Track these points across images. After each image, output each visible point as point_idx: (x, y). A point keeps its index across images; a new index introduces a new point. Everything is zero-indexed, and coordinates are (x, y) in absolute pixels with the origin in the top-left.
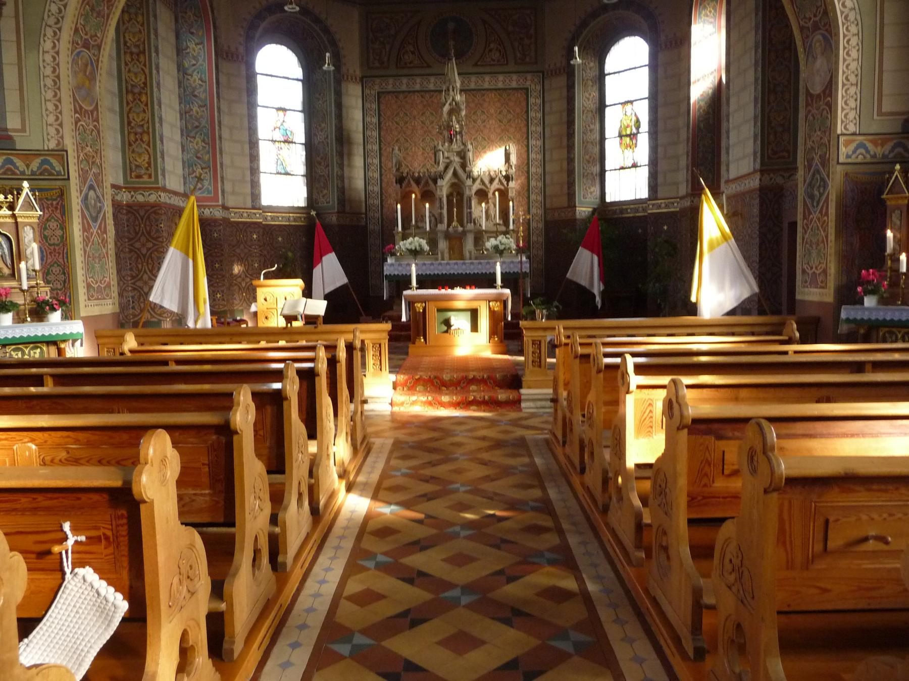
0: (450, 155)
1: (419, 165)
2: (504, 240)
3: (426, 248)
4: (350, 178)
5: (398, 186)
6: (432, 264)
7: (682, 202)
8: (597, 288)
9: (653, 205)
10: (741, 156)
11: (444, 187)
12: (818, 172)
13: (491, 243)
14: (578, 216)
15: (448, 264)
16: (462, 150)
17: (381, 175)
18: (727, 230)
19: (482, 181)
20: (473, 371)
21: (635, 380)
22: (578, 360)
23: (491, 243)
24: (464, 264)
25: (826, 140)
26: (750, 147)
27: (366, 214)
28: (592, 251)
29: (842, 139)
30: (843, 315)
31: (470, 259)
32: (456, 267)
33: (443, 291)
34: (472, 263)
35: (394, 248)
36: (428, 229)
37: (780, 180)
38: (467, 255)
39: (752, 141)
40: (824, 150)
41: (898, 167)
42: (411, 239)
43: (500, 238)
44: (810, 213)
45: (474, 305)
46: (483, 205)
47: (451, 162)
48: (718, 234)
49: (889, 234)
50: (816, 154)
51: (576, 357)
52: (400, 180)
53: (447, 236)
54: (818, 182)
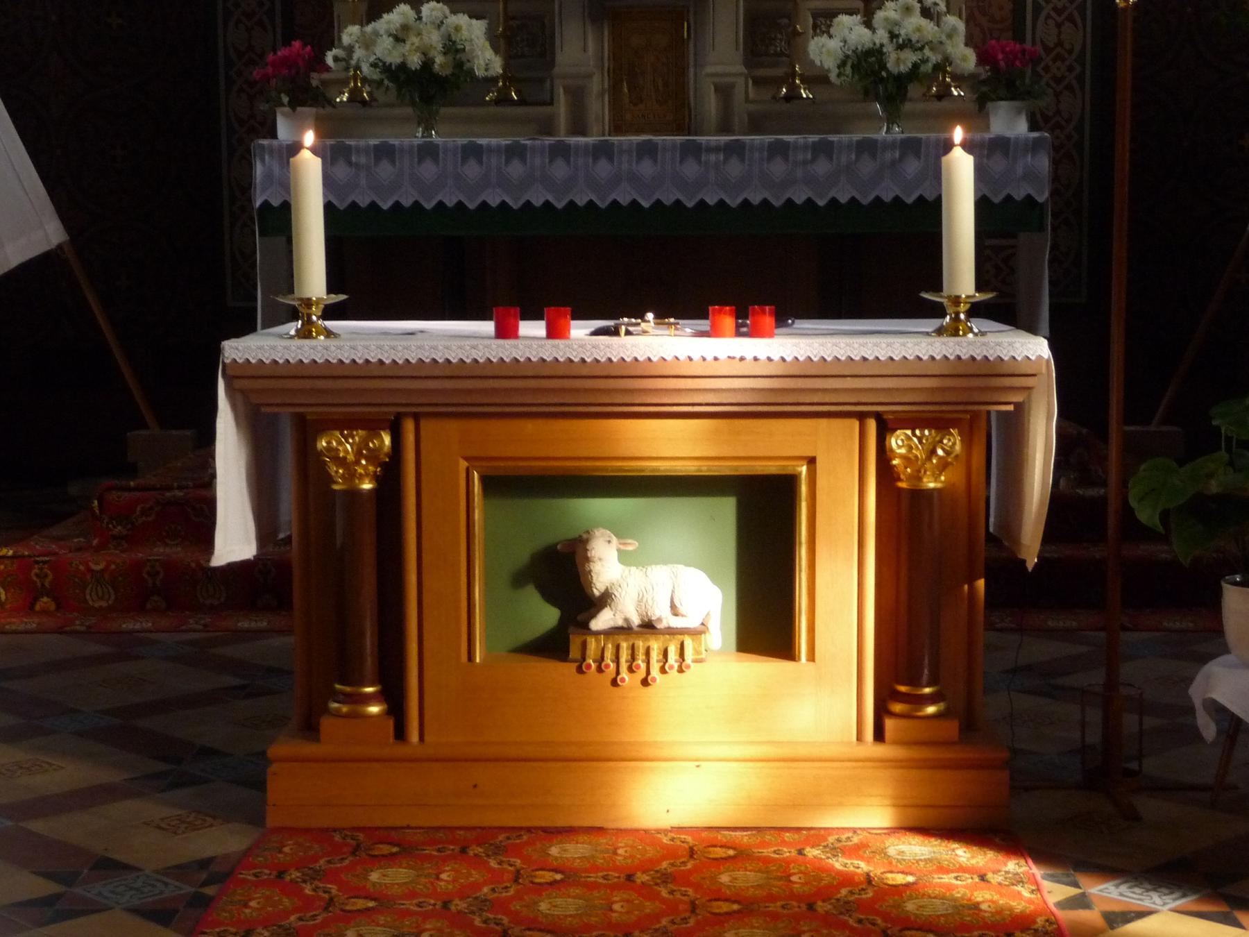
6: (515, 152)
15: (603, 151)
24: (693, 151)
31: (725, 128)
32: (646, 168)
34: (734, 150)
38: (711, 105)
45: (769, 447)
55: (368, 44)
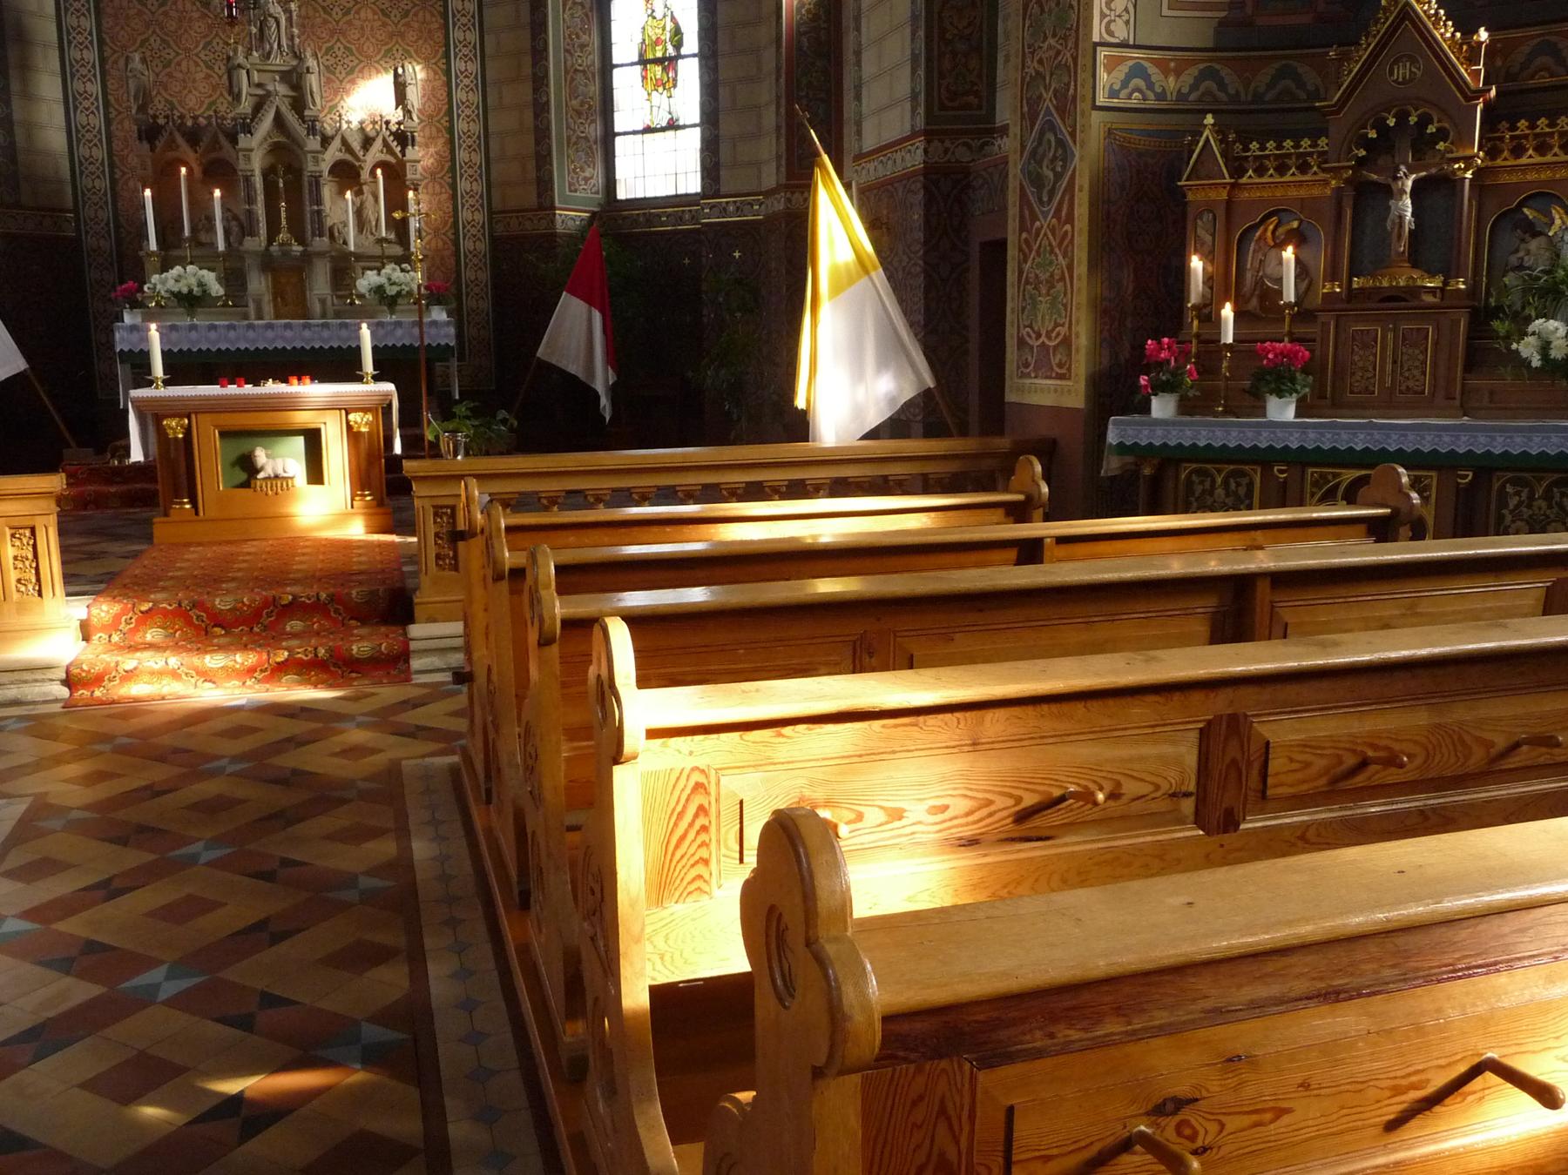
0: (266, 78)
1: (196, 99)
2: (398, 275)
3: (217, 289)
4: (30, 127)
5: (146, 146)
7: (769, 202)
8: (601, 379)
9: (712, 207)
10: (886, 92)
11: (254, 153)
12: (1052, 127)
13: (367, 281)
14: (560, 228)
15: (270, 326)
16: (294, 68)
17: (108, 122)
18: (868, 247)
19: (344, 142)
20: (296, 582)
21: (642, 707)
22: (504, 586)
23: (367, 281)
25: (1067, 56)
26: (903, 84)
27: (76, 210)
28: (590, 302)
29: (1102, 53)
30: (1112, 437)
31: (324, 316)
32: (288, 334)
33: (232, 389)
35: (141, 290)
36: (221, 246)
37: (963, 155)
38: (317, 308)
39: (907, 69)
40: (1066, 80)
41: (1209, 119)
42: (177, 270)
43: (389, 269)
44: (1034, 218)
46: (348, 195)
47: (269, 94)
48: (848, 257)
49: (1196, 263)
50: (1047, 89)
51: (498, 577)
52: (150, 133)
53: (268, 264)
54: (1051, 148)
55: (164, 282)
